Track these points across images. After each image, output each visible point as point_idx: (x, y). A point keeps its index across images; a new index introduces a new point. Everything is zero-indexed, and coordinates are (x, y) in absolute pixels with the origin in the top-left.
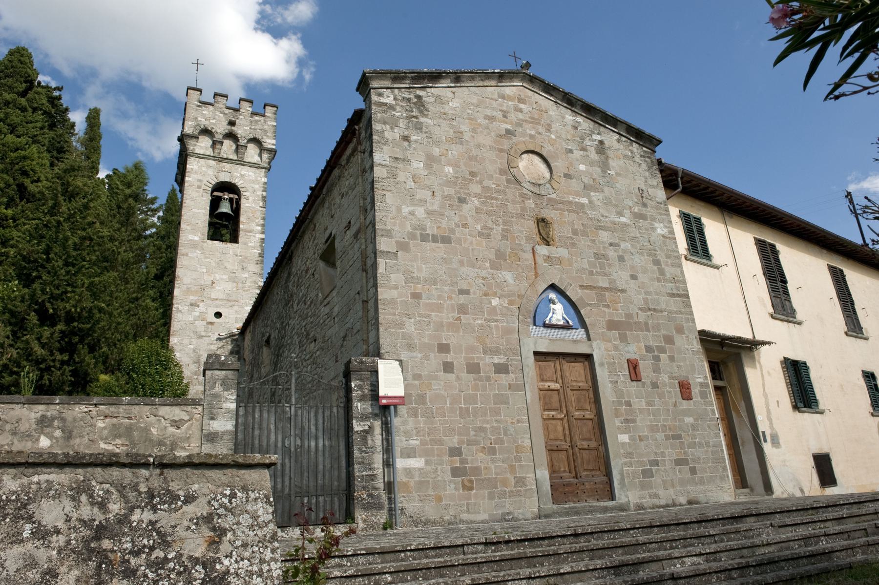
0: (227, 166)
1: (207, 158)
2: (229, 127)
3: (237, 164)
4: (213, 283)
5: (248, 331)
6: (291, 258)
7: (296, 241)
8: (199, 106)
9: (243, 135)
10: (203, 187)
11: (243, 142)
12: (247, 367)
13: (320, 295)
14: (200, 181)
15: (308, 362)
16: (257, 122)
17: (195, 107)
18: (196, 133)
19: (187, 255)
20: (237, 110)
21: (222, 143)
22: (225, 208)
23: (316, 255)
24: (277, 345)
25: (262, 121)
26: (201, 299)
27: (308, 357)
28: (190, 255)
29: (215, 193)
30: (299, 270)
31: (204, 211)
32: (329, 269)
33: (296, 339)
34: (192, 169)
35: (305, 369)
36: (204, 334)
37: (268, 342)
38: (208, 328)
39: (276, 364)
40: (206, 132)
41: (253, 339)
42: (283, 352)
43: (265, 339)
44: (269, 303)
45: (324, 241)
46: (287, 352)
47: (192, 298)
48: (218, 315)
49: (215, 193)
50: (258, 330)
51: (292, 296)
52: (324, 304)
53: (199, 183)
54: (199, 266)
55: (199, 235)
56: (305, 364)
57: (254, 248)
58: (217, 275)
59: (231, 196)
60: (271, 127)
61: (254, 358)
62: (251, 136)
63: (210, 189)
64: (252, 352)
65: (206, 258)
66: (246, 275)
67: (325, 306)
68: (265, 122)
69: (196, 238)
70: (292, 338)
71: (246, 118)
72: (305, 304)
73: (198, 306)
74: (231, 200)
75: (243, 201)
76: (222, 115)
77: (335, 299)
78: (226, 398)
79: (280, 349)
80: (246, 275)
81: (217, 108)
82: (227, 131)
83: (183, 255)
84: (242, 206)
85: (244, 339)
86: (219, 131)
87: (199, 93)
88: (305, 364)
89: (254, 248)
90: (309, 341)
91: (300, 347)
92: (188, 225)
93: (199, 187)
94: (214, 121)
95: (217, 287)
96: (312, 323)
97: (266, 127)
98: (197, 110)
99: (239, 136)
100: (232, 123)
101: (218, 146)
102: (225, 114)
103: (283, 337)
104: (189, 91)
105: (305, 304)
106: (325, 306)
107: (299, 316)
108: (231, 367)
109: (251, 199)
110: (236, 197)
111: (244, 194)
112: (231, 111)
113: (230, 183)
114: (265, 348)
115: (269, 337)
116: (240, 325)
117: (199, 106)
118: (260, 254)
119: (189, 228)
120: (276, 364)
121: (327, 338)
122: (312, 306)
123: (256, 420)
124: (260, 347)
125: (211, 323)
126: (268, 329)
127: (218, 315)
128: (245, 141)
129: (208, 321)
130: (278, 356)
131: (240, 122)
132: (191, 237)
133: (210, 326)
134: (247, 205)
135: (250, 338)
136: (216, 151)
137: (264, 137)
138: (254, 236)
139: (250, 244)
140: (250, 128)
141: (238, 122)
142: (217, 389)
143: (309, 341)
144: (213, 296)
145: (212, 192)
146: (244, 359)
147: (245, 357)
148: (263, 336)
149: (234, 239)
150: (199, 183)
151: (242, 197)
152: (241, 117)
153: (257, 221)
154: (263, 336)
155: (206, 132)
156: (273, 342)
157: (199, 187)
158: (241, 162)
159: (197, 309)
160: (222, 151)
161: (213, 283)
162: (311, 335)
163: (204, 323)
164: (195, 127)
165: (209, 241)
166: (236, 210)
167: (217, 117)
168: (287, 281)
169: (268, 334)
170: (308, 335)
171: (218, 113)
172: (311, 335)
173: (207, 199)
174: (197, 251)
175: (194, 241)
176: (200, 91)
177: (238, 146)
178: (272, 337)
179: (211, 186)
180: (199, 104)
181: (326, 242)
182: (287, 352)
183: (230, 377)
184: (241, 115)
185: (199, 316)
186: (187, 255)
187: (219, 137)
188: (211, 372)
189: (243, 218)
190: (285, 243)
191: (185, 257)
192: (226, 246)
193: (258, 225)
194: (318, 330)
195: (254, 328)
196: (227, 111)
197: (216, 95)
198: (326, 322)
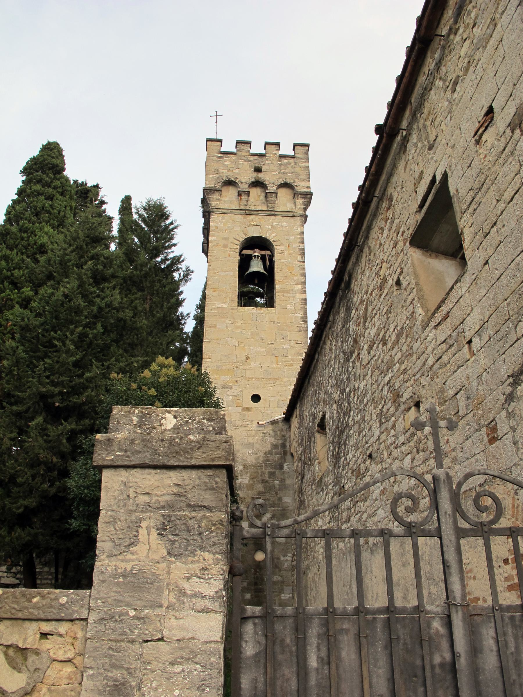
0: (254, 219)
1: (231, 213)
2: (255, 175)
3: (268, 215)
4: (247, 358)
5: (294, 416)
6: (348, 285)
7: (356, 251)
8: (220, 157)
9: (272, 181)
10: (230, 245)
11: (271, 189)
12: (296, 465)
13: (420, 310)
14: (226, 239)
15: (403, 448)
16: (286, 165)
17: (215, 158)
18: (218, 186)
19: (215, 327)
20: (261, 155)
21: (248, 194)
22: (256, 266)
23: (401, 244)
24: (338, 428)
25: (293, 164)
26: (234, 379)
27: (402, 439)
28: (218, 326)
29: (245, 252)
30: (366, 292)
31: (231, 273)
32: (430, 260)
33: (372, 411)
34: (216, 227)
35: (397, 463)
36: (239, 423)
37: (322, 426)
38: (244, 415)
39: (337, 458)
40: (229, 183)
41: (300, 426)
42: (348, 437)
43: (317, 422)
44: (320, 367)
45: (415, 206)
46: (355, 436)
47: (223, 378)
48: (256, 398)
49: (245, 252)
50: (307, 413)
51: (356, 341)
52: (432, 324)
53: (225, 242)
54: (230, 339)
55: (228, 301)
56: (396, 453)
57: (295, 311)
58: (251, 348)
59: (263, 253)
60: (303, 169)
61: (304, 452)
62: (281, 181)
63: (238, 247)
64: (301, 443)
65: (238, 328)
66: (287, 346)
67: (436, 326)
68: (296, 163)
69: (225, 306)
70: (362, 410)
71: (274, 162)
72: (385, 344)
73: (231, 388)
74: (263, 258)
75: (277, 259)
76: (246, 163)
77: (467, 299)
78: (182, 592)
79: (342, 432)
80: (287, 346)
81: (240, 156)
82: (253, 180)
83: (210, 327)
84: (276, 263)
85: (290, 427)
86: (243, 181)
87: (219, 143)
88: (396, 453)
89: (295, 311)
90: (402, 407)
91: (381, 424)
92: (214, 291)
93: (225, 246)
94: (237, 171)
95: (253, 364)
96: (405, 372)
97: (297, 169)
98: (217, 161)
99: (267, 183)
100: (258, 170)
101: (244, 198)
102: (249, 161)
103: (347, 413)
104: (209, 143)
105: (385, 344)
106: (436, 326)
107: (375, 369)
108: (198, 458)
109: (286, 253)
110: (269, 253)
111: (277, 248)
112: (256, 157)
113: (260, 238)
114: (317, 435)
115: (323, 419)
116: (284, 409)
117: (220, 157)
118: (302, 318)
119: (215, 294)
120: (337, 458)
121: (452, 392)
122: (402, 340)
123: (313, 680)
124: (311, 435)
125: (248, 409)
126: (320, 407)
127: (256, 398)
128: (275, 188)
129: (244, 406)
130: (339, 444)
131: (268, 168)
132: (219, 305)
133: (246, 413)
134: (283, 261)
135: (297, 426)
136: (243, 203)
137: (296, 180)
138: (294, 297)
139: (289, 307)
140: (280, 173)
141: (264, 168)
142: (141, 550)
143: (402, 407)
144: (248, 374)
145: (241, 251)
146: (292, 455)
147: (292, 451)
148: (314, 418)
149: (270, 303)
150: (225, 242)
151: (276, 252)
152: (267, 162)
153: (296, 278)
154: (314, 418)
155: (229, 183)
156: (330, 424)
157: (225, 246)
158: (271, 213)
159: (230, 392)
160: (249, 203)
161: (247, 358)
162: (406, 395)
163: (240, 409)
164: (216, 180)
165: (240, 308)
166: (270, 268)
167: (240, 166)
168: (347, 320)
169: (320, 415)
170: (398, 396)
171: (241, 162)
172: (406, 395)
173: (236, 259)
174: (227, 321)
175: (223, 309)
176: (220, 141)
177: (266, 193)
178: (327, 417)
179: (239, 243)
180: (220, 155)
181: (421, 206)
182: (355, 436)
183: (194, 497)
184: (267, 160)
185: (232, 401)
186: (215, 327)
187: (244, 187)
188: (124, 475)
189: (278, 276)
190: (338, 260)
191: (213, 329)
192: (261, 312)
193: (297, 284)
194: (425, 380)
195: (302, 411)
196: (252, 158)
197: (238, 143)
198: (445, 358)
